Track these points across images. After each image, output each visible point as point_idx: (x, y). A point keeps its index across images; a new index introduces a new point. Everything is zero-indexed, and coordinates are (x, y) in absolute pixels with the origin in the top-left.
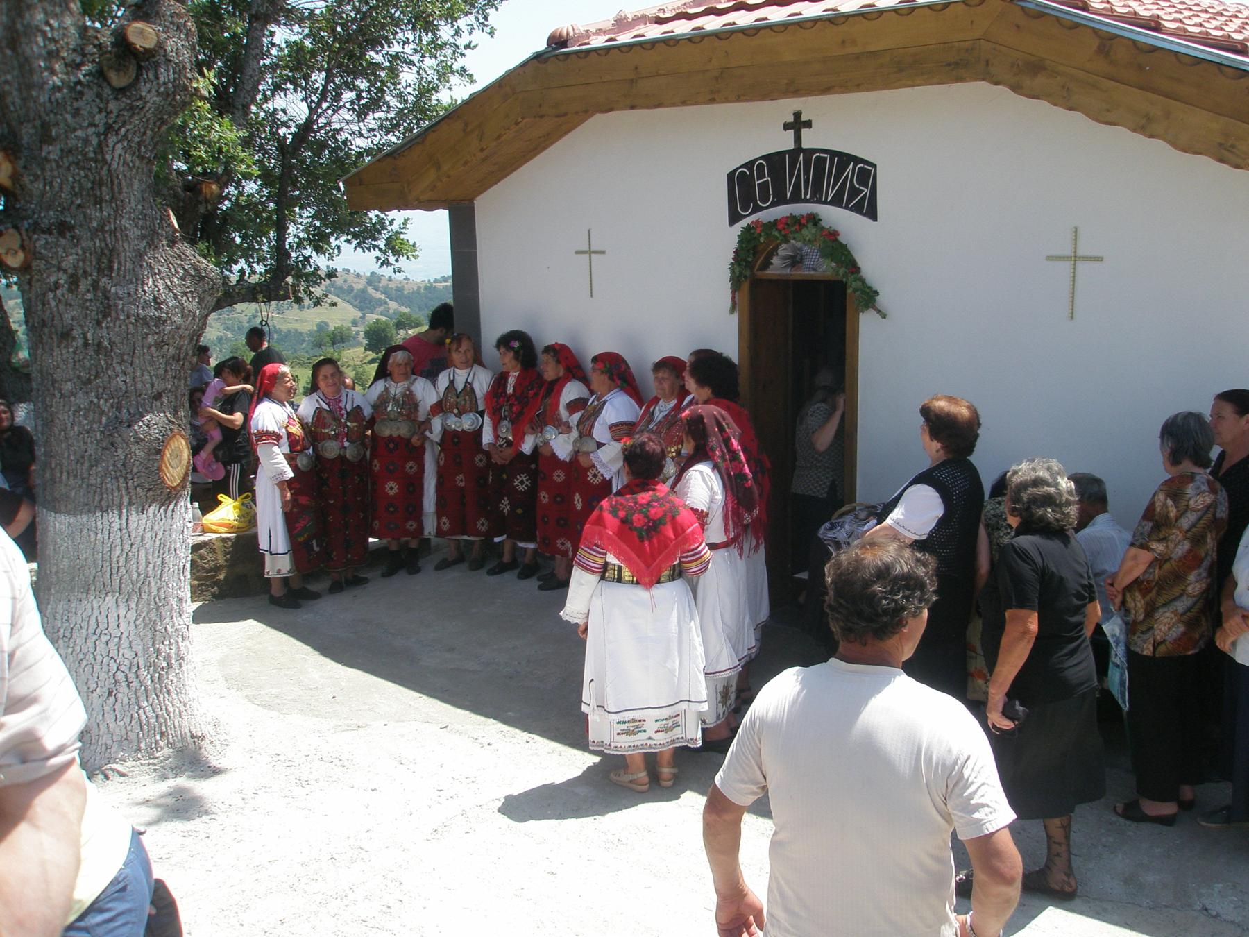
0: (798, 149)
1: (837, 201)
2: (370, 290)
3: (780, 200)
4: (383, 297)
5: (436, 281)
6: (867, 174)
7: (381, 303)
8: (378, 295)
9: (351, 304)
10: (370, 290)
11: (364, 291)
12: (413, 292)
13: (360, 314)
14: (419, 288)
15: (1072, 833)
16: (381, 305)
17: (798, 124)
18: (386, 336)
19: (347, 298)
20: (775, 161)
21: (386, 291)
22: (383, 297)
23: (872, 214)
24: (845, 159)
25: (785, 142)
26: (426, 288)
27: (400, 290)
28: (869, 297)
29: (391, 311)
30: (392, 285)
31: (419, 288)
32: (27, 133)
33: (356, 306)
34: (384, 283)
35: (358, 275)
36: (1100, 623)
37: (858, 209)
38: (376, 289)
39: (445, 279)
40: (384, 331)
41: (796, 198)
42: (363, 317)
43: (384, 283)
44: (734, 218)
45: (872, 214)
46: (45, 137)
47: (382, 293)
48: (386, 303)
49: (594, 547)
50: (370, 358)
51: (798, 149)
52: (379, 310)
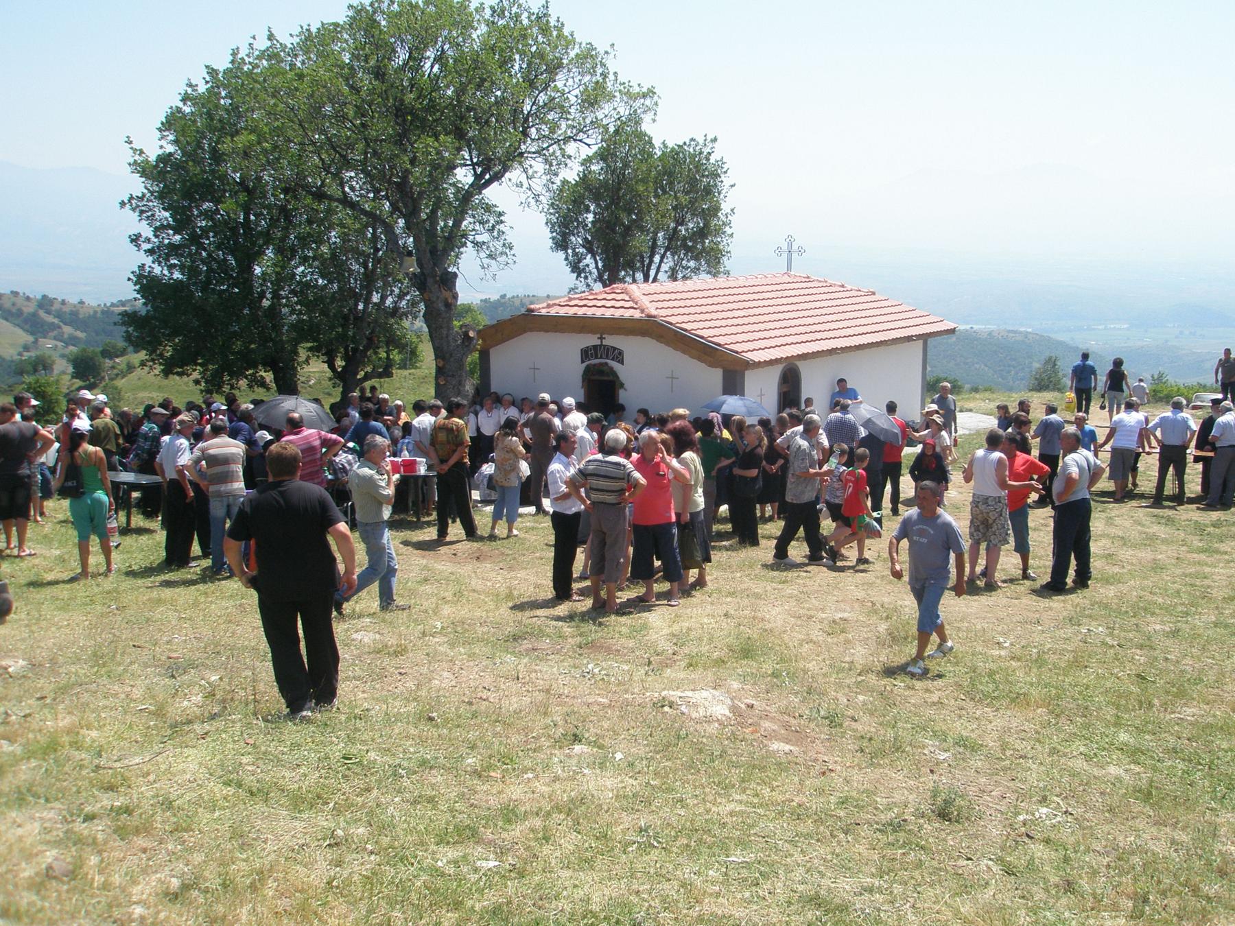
0: (601, 345)
1: (613, 359)
2: (42, 313)
3: (596, 358)
4: (56, 321)
5: (113, 305)
6: (621, 353)
7: (53, 327)
8: (50, 319)
9: (22, 328)
10: (42, 313)
11: (35, 315)
12: (89, 317)
13: (31, 339)
14: (96, 312)
15: (365, 591)
16: (53, 330)
17: (601, 338)
18: (94, 364)
19: (16, 322)
20: (595, 347)
21: (59, 315)
22: (56, 321)
23: (623, 364)
24: (615, 349)
25: (598, 342)
26: (103, 312)
27: (74, 313)
28: (622, 385)
29: (66, 336)
30: (66, 309)
31: (96, 312)
32: (447, 356)
33: (27, 331)
34: (56, 306)
35: (28, 298)
36: (305, 423)
37: (619, 362)
38: (49, 312)
39: (1095, 519)
40: (92, 359)
41: (601, 358)
42: (36, 342)
43: (56, 306)
44: (583, 362)
45: (623, 364)
46: (451, 355)
47: (55, 317)
48: (60, 327)
49: (983, 546)
50: (76, 386)
51: (601, 345)
52: (52, 334)
